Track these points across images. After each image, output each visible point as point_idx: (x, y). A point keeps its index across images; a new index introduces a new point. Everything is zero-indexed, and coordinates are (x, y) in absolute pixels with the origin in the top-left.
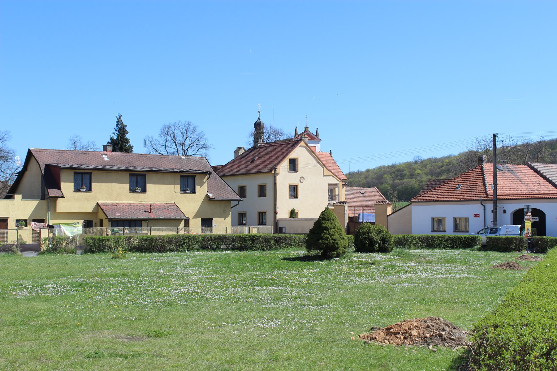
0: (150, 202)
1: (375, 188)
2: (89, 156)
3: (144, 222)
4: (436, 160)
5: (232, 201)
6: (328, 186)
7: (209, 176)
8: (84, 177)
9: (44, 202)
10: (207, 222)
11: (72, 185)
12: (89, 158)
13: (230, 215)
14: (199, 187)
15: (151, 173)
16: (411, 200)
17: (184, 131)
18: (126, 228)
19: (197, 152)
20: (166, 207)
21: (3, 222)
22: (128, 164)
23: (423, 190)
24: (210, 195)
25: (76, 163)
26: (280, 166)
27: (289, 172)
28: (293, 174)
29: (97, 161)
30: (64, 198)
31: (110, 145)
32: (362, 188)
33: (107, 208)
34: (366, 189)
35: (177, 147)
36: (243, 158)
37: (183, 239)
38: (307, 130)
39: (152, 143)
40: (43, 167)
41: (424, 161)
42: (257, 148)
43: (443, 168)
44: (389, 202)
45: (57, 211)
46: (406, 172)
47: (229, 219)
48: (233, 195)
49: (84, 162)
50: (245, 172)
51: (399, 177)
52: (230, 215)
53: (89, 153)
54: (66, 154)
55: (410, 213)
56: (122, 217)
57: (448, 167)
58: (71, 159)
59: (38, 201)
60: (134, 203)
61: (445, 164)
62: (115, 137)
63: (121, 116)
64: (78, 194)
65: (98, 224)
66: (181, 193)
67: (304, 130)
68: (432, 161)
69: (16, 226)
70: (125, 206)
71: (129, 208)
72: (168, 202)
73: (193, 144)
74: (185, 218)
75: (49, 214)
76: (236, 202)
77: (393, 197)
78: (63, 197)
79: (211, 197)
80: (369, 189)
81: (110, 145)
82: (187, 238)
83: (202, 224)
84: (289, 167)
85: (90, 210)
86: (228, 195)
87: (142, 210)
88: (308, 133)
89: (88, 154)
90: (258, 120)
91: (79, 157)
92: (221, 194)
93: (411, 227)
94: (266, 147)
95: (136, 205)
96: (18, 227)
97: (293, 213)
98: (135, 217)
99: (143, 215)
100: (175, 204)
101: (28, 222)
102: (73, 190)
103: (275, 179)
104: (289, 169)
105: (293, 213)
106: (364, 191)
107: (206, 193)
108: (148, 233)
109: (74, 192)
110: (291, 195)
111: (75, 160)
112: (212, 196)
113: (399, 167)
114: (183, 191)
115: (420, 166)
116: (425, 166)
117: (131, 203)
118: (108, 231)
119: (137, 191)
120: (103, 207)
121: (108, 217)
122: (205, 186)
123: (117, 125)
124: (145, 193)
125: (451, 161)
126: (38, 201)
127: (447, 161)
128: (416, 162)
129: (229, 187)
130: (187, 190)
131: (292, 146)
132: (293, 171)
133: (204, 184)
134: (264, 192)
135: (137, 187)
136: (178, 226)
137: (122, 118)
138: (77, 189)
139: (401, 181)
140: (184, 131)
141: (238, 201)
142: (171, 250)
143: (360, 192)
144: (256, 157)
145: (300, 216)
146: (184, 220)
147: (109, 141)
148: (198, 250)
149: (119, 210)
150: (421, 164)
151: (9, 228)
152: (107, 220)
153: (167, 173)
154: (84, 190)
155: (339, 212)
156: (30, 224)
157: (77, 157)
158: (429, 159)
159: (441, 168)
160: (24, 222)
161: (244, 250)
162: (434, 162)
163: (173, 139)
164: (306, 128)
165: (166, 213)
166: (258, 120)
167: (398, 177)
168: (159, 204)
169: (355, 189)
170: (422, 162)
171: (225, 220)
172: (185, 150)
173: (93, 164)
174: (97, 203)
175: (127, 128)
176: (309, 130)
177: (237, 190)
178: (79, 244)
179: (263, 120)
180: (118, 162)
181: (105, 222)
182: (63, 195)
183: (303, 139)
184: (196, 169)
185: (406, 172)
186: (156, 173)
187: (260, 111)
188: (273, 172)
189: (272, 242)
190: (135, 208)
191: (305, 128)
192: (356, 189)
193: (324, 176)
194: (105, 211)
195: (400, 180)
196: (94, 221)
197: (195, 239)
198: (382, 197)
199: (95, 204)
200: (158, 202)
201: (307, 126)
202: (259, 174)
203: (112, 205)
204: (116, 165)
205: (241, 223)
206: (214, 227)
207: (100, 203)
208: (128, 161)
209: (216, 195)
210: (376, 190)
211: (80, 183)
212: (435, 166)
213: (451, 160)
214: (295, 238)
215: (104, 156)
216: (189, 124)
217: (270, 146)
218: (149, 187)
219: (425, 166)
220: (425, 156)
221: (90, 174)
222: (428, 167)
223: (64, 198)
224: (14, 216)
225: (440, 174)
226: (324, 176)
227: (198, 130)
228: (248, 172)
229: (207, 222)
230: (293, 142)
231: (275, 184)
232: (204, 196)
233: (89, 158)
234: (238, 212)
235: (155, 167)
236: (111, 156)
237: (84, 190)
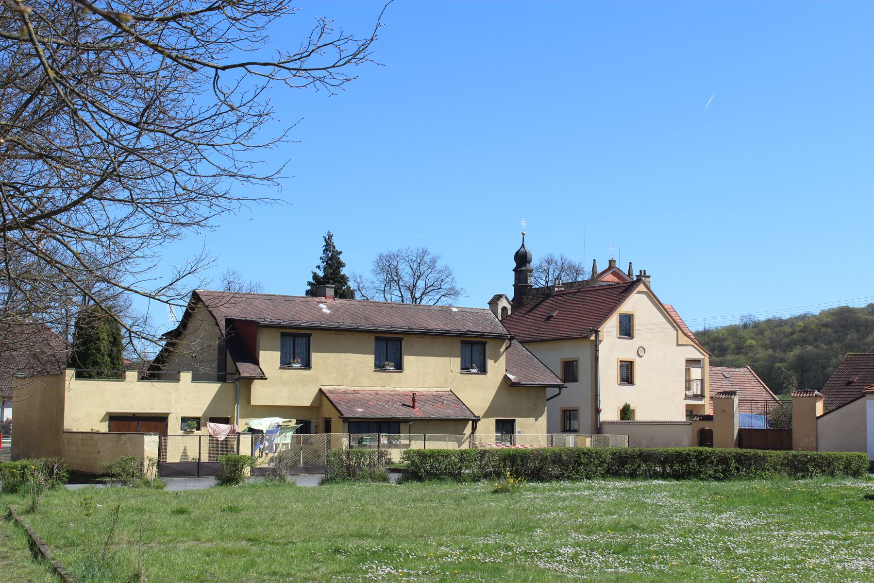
0: (409, 389)
1: (748, 369)
2: (296, 304)
3: (404, 424)
4: (781, 323)
5: (547, 388)
6: (686, 363)
7: (510, 343)
8: (296, 342)
9: (229, 386)
10: (506, 427)
11: (278, 354)
12: (297, 308)
13: (545, 414)
14: (493, 361)
15: (412, 336)
16: (866, 389)
17: (415, 266)
18: (384, 434)
19: (438, 302)
20: (437, 398)
21: (160, 421)
22: (364, 320)
23: (838, 373)
24: (510, 376)
25: (277, 316)
26: (603, 328)
27: (619, 338)
28: (627, 342)
29: (311, 314)
30: (266, 379)
31: (331, 286)
32: (727, 369)
33: (338, 398)
34: (732, 369)
35: (401, 293)
36: (527, 313)
37: (579, 457)
38: (612, 266)
39: (361, 286)
40: (222, 324)
41: (760, 324)
42: (552, 296)
43: (795, 336)
44: (819, 393)
45: (252, 404)
46: (730, 343)
47: (543, 420)
48: (549, 377)
49: (289, 315)
51: (716, 352)
52: (545, 414)
53: (297, 299)
54: (258, 301)
55: (863, 414)
56: (367, 416)
57: (803, 334)
58: (267, 309)
59: (220, 385)
60: (382, 391)
61: (798, 329)
62: (321, 274)
63: (332, 236)
64: (287, 373)
65: (322, 426)
66: (461, 373)
67: (607, 267)
68: (774, 324)
69: (181, 430)
70: (367, 395)
71: (376, 398)
72: (440, 389)
73: (431, 288)
74: (473, 418)
75: (237, 408)
76: (557, 391)
77: (789, 384)
78: (263, 378)
79: (513, 381)
80: (737, 370)
81: (331, 286)
82: (585, 454)
83: (497, 430)
84: (618, 328)
86: (541, 377)
87: (398, 403)
88: (614, 271)
89: (295, 301)
90: (522, 249)
91: (279, 307)
92: (528, 375)
93: (866, 438)
94: (570, 293)
95: (386, 393)
96: (185, 430)
97: (626, 412)
98: (389, 416)
99: (402, 413)
100: (452, 393)
101: (202, 421)
102: (279, 365)
103: (596, 350)
104: (618, 333)
105: (626, 412)
106: (730, 373)
107: (504, 373)
108: (409, 445)
109: (280, 368)
110: (622, 379)
111: (275, 312)
112: (515, 379)
113: (717, 334)
114: (465, 369)
115: (752, 332)
116: (761, 333)
117: (377, 389)
118: (343, 441)
119: (388, 368)
120: (331, 396)
121: (343, 415)
122: (503, 360)
123: (325, 251)
124: (401, 372)
125: (808, 324)
126: (220, 385)
127: (801, 324)
128: (745, 326)
129: (540, 364)
130: (472, 368)
131: (623, 292)
132: (625, 336)
133: (501, 355)
134: (573, 371)
135: (387, 361)
136: (461, 432)
137: (334, 240)
138: (286, 363)
139: (721, 358)
140: (415, 266)
141: (560, 387)
142: (558, 478)
143: (724, 376)
144: (556, 310)
145: (639, 417)
146: (471, 422)
147: (311, 280)
148: (603, 477)
150: (755, 330)
151: (170, 432)
152: (341, 420)
153: (438, 337)
155: (724, 411)
156: (206, 426)
157: (276, 307)
158: (769, 321)
159: (791, 336)
160: (195, 422)
161: (684, 479)
162: (777, 327)
163: (396, 279)
164: (611, 262)
165: (440, 409)
166: (522, 249)
167: (715, 352)
168: (425, 393)
169: (714, 369)
170: (756, 325)
171: (536, 421)
172: (416, 299)
173: (306, 319)
174: (320, 389)
175: (342, 258)
176: (617, 265)
177: (559, 370)
178: (303, 463)
179: (529, 248)
180: (346, 316)
181: (336, 423)
182: (264, 374)
183: (643, 278)
184: (478, 330)
185: (727, 343)
186: (420, 336)
187: (524, 233)
188: (593, 338)
189: (733, 464)
190: (386, 399)
191: (610, 262)
192: (716, 369)
193: (678, 345)
194: (336, 404)
195: (718, 357)
197: (600, 457)
198: (761, 384)
199: (317, 390)
200: (423, 389)
201: (614, 259)
202: (566, 341)
203: (345, 392)
204: (343, 321)
205: (567, 429)
206: (517, 436)
207: (324, 388)
208: (364, 314)
209: (522, 378)
210: (750, 372)
211: (290, 354)
212: (780, 332)
213: (807, 322)
214: (770, 456)
215: (321, 305)
216: (425, 252)
217: (579, 291)
219: (761, 333)
220: (762, 315)
221: (309, 336)
222: (766, 335)
223: (266, 379)
224: (179, 412)
225: (790, 346)
226: (678, 345)
227: (440, 265)
228: (544, 338)
229: (506, 427)
230: (624, 285)
231: (596, 359)
232: (500, 378)
233: (297, 308)
234: (561, 408)
235: (409, 325)
236: (334, 306)
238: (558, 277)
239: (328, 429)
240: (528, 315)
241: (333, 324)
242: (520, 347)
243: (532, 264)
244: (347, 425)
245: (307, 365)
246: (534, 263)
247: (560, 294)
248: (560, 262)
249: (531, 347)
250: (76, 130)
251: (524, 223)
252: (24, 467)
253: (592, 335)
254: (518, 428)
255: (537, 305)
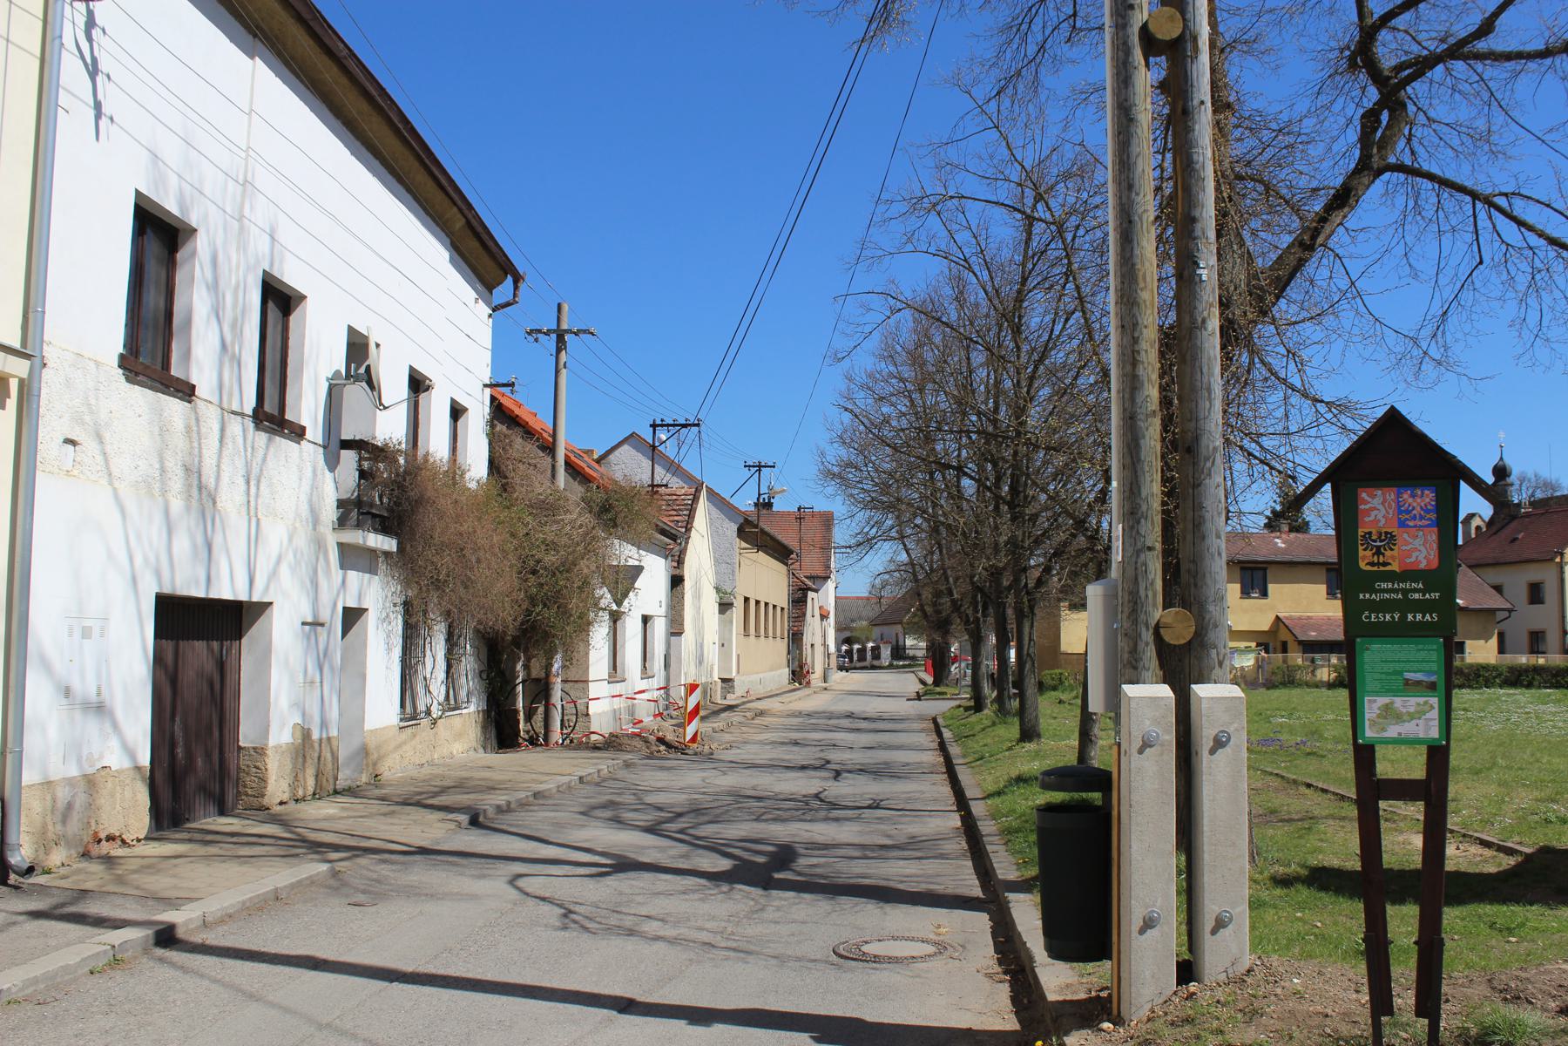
11: (1238, 586)
50: (1502, 560)
56: (1320, 639)
76: (1507, 614)
85: (1266, 627)
102: (1239, 595)
103: (1562, 572)
118: (1297, 659)
120: (1286, 622)
138: (1245, 593)
149: (1316, 627)
154: (1256, 595)
179: (1508, 461)
181: (1291, 645)
188: (1558, 560)
196: (1271, 645)
199: (1274, 617)
203: (1300, 618)
207: (1280, 615)
215: (1277, 540)
218: (1272, 588)
231: (1562, 581)
237: (1256, 595)
238: (1533, 495)
239: (1285, 650)
240: (1494, 537)
241: (1287, 558)
242: (1470, 573)
243: (1512, 477)
244: (1301, 647)
245: (1264, 594)
246: (1513, 478)
247: (1528, 515)
248: (1533, 479)
249: (1479, 571)
250: (1019, 73)
251: (1502, 435)
252: (1061, 674)
253: (1556, 557)
254: (1468, 649)
255: (1503, 527)
